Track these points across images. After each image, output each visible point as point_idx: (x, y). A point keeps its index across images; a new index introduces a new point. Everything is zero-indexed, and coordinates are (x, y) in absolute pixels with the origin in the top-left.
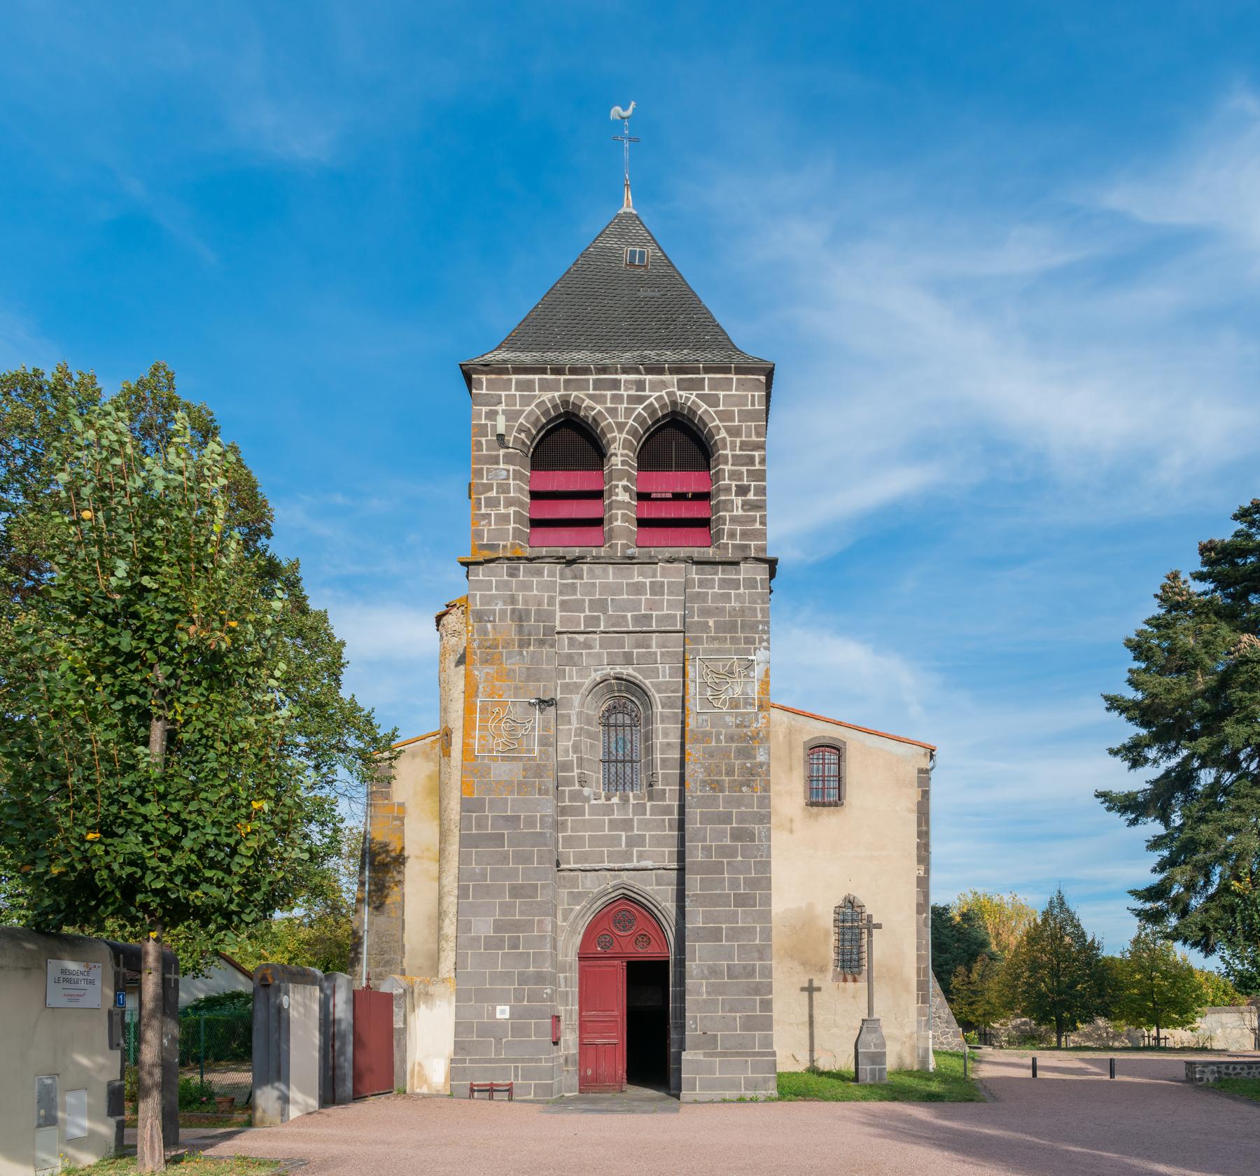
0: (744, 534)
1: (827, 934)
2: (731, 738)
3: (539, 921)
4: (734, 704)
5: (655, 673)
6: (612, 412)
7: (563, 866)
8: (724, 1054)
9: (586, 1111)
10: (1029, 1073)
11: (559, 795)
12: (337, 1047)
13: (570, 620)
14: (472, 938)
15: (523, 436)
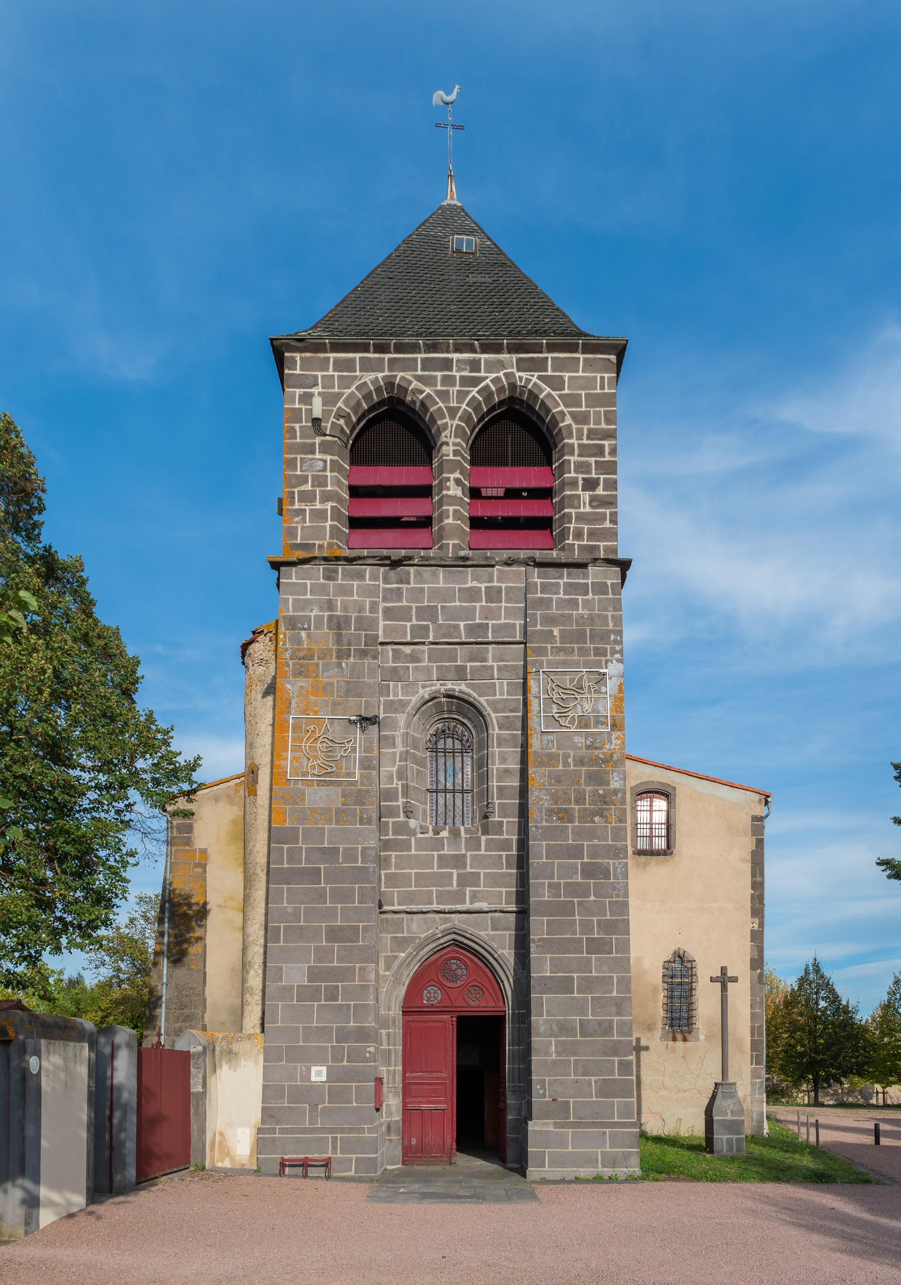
0: (592, 534)
1: (655, 989)
2: (580, 761)
3: (361, 969)
4: (584, 722)
5: (492, 689)
6: (444, 395)
7: (385, 908)
8: (578, 1125)
9: (424, 1196)
10: (870, 1140)
11: (382, 828)
12: (115, 1121)
13: (394, 629)
14: (284, 988)
15: (342, 422)
